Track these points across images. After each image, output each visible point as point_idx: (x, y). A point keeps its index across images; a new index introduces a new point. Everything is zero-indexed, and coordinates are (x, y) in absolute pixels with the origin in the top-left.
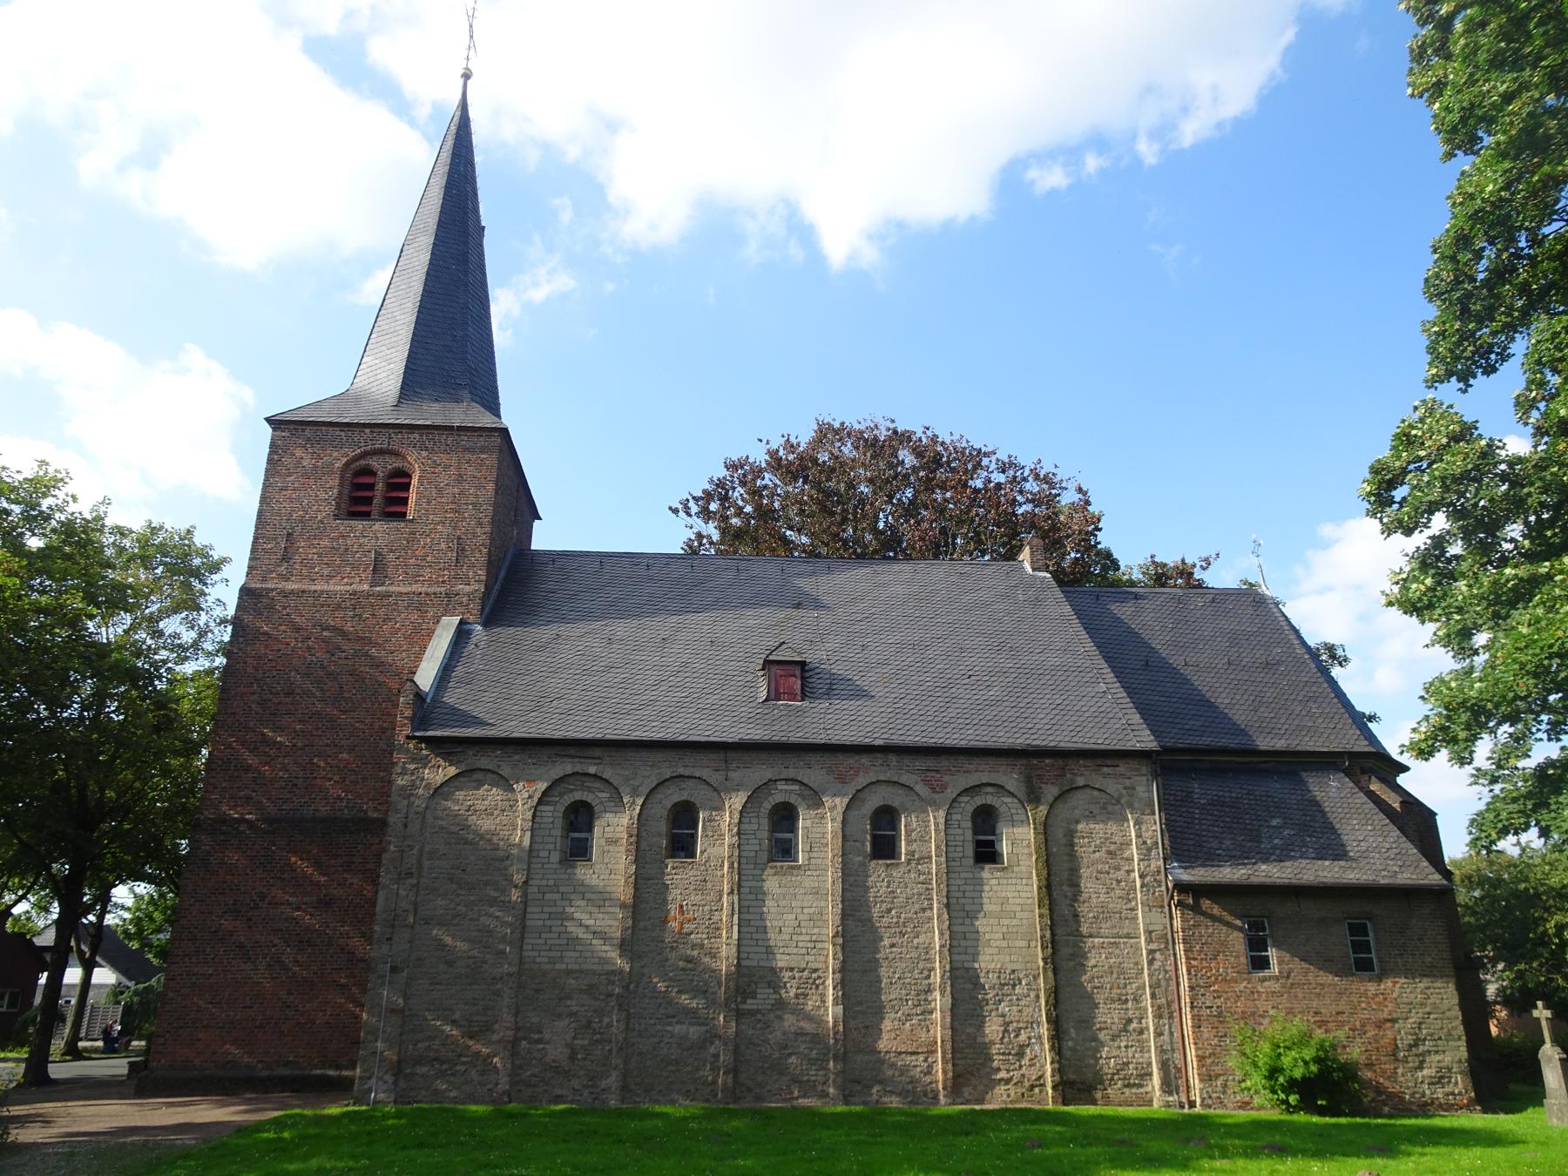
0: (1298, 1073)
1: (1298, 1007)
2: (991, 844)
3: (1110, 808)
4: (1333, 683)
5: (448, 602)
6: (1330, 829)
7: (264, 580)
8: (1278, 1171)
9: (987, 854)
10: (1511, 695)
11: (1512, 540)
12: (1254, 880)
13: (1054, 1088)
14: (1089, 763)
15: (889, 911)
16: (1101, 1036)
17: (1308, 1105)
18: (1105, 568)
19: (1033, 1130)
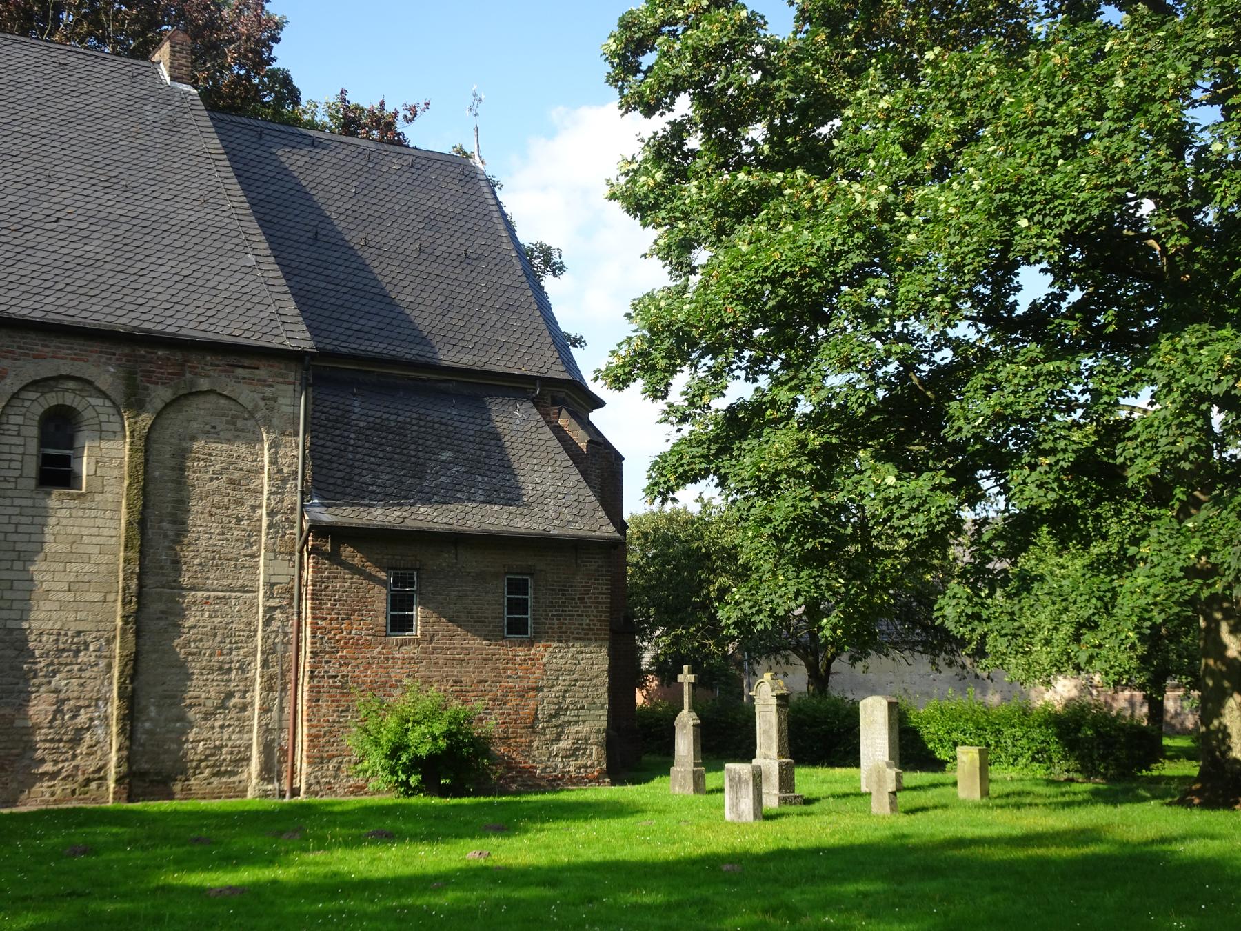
0: (423, 751)
1: (437, 674)
2: (66, 460)
3: (240, 423)
4: (539, 292)
6: (507, 467)
8: (380, 859)
9: (57, 473)
10: (718, 320)
11: (753, 143)
12: (410, 524)
13: (117, 781)
14: (219, 360)
16: (191, 714)
17: (430, 786)
18: (280, 100)
19: (79, 836)
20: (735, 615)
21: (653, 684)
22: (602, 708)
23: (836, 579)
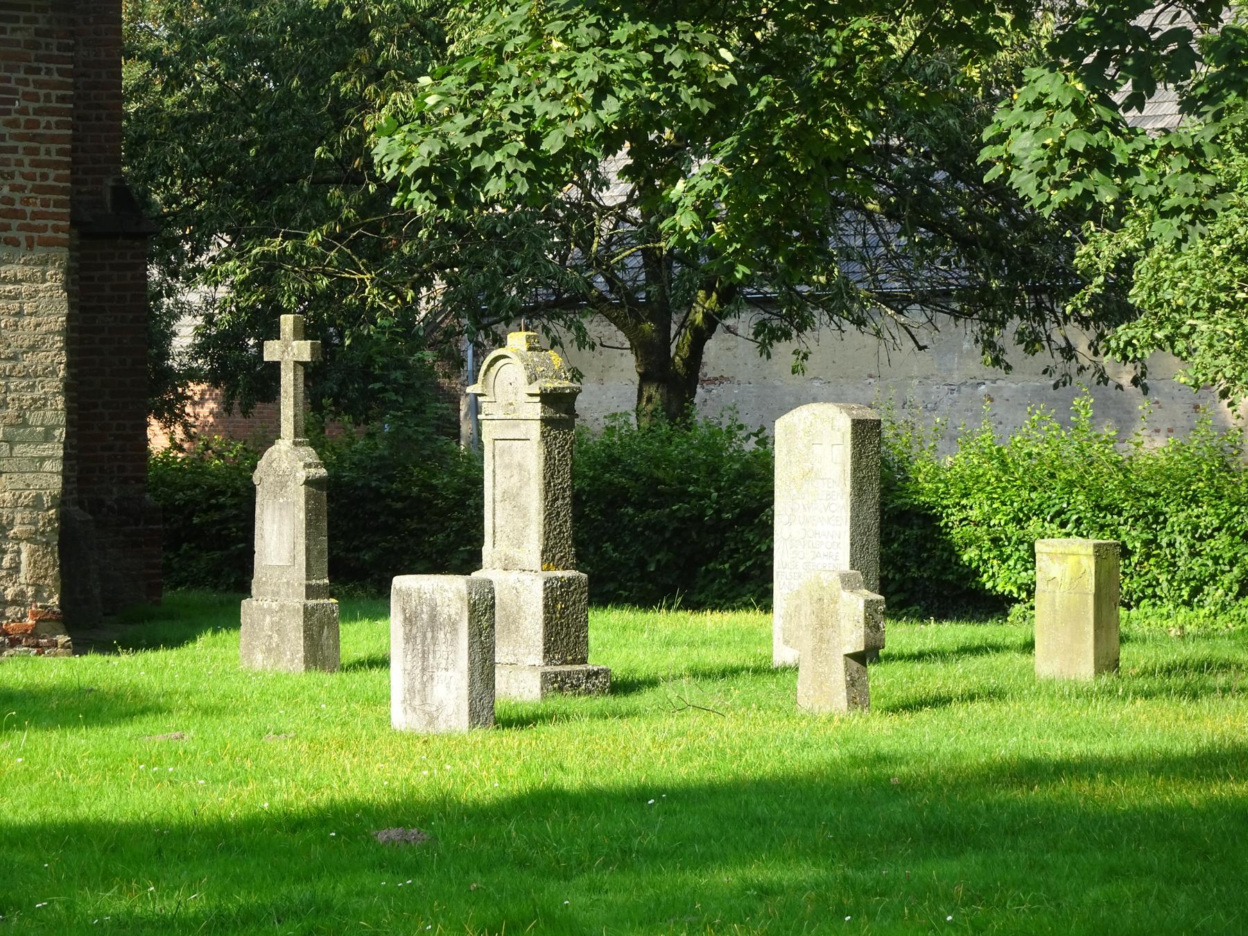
20: (425, 152)
21: (204, 411)
22: (48, 436)
23: (712, 52)
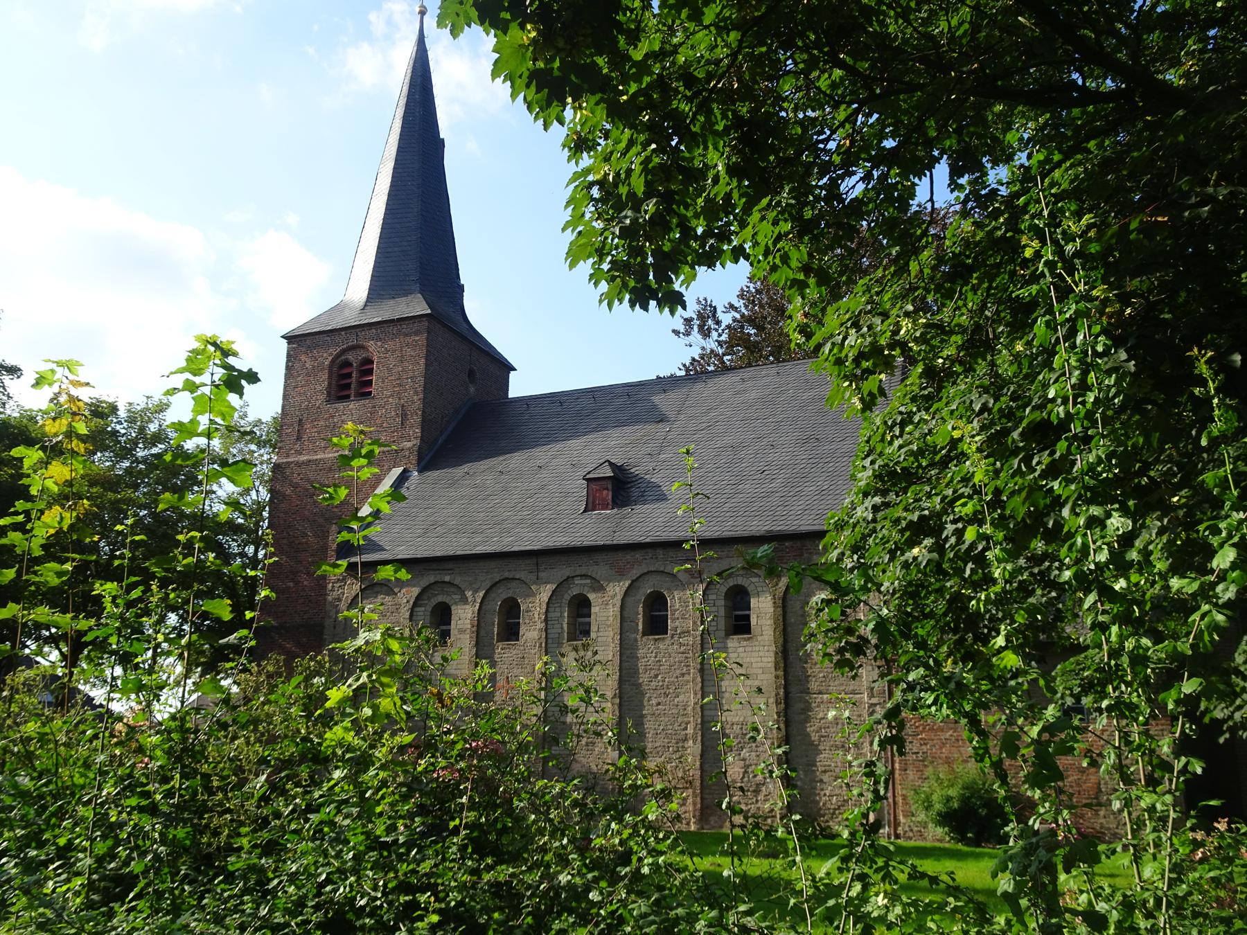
5: (394, 458)
7: (288, 456)
15: (656, 676)
